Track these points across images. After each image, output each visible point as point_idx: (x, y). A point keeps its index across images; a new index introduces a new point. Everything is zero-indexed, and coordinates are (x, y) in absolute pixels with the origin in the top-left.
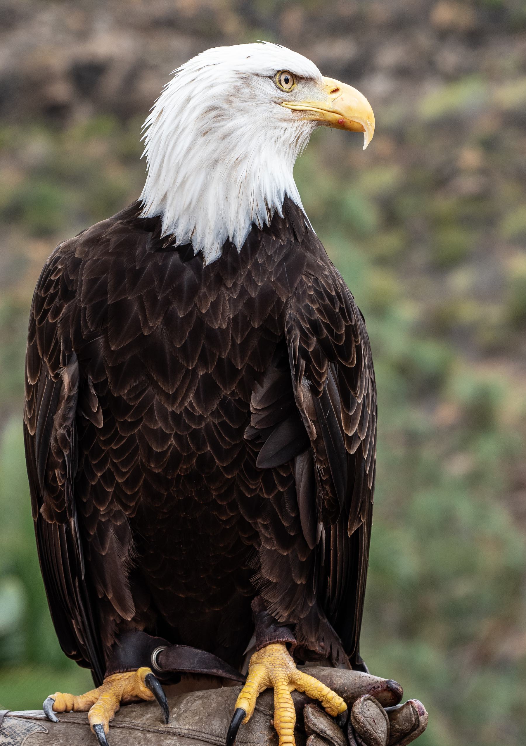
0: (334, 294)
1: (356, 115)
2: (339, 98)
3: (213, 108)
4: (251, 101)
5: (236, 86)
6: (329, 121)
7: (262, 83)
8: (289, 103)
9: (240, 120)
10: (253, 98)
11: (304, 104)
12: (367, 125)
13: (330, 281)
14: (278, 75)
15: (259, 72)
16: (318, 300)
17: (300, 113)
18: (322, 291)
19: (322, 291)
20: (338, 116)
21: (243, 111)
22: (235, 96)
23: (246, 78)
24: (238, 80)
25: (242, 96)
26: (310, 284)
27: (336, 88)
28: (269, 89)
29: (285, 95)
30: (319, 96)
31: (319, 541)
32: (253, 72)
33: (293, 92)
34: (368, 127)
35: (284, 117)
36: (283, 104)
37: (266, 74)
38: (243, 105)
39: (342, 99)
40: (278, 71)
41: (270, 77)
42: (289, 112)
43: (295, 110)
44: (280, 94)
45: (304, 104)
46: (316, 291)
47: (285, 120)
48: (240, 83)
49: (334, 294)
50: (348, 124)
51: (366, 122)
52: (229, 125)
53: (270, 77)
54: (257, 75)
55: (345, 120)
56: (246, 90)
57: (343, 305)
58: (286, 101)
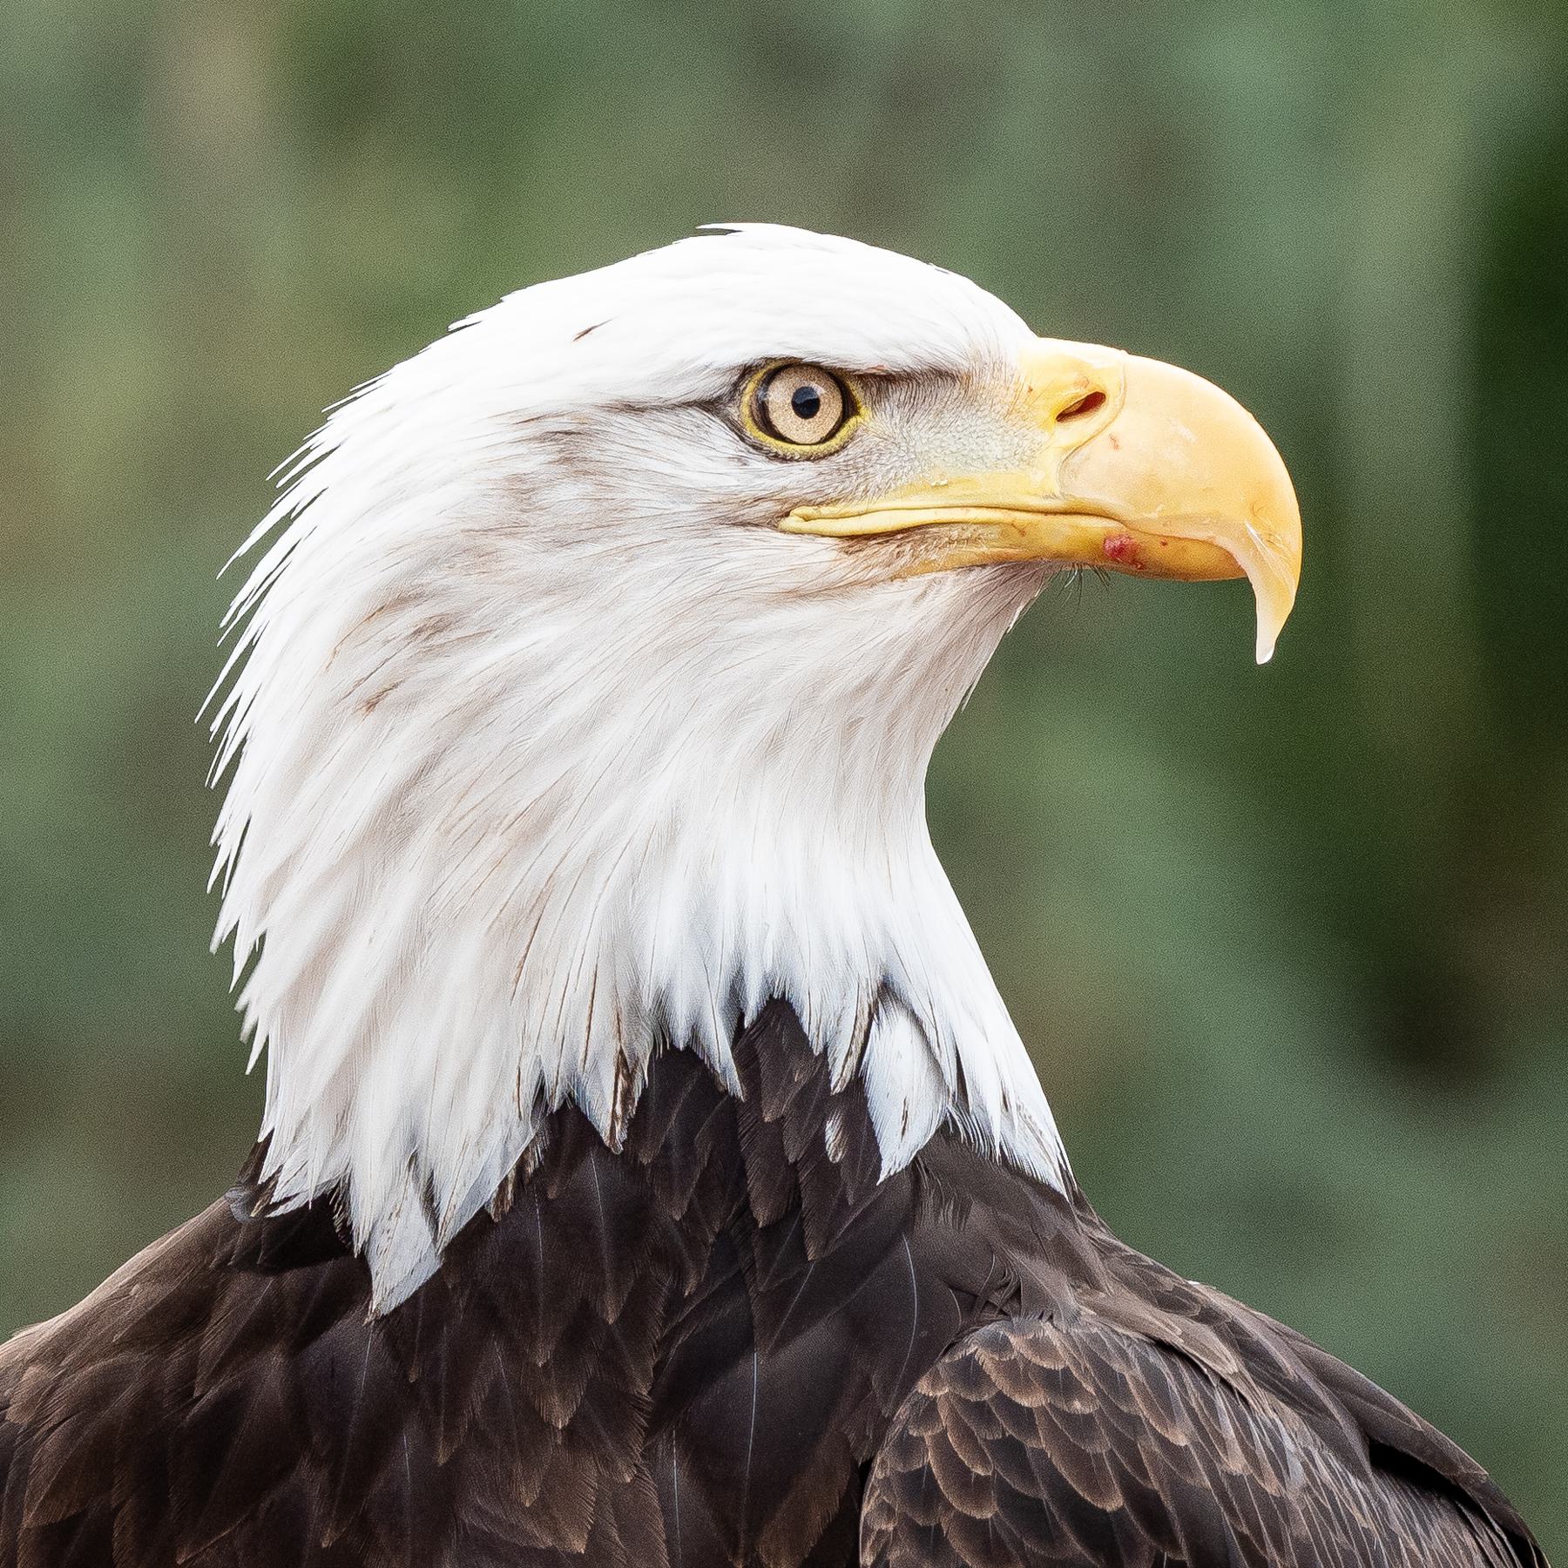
0: (1115, 1502)
1: (1188, 508)
2: (1102, 440)
3: (399, 601)
4: (596, 540)
5: (518, 478)
6: (1058, 555)
7: (657, 442)
8: (825, 510)
9: (539, 634)
10: (607, 521)
11: (915, 501)
12: (1250, 543)
13: (1101, 1446)
14: (750, 387)
15: (634, 394)
16: (1020, 1546)
17: (892, 547)
18: (1044, 1496)
19: (1044, 1496)
20: (1095, 527)
21: (562, 589)
22: (512, 530)
23: (568, 439)
24: (522, 449)
25: (546, 520)
26: (980, 1471)
27: (1084, 393)
28: (712, 461)
29: (797, 477)
30: (996, 449)
31: (243, 549)
32: (601, 401)
33: (852, 450)
34: (1258, 557)
35: (789, 583)
36: (791, 522)
37: (675, 393)
38: (560, 562)
39: (1113, 439)
40: (747, 371)
41: (710, 405)
42: (820, 557)
43: (858, 540)
44: (765, 477)
45: (915, 501)
46: (1009, 1499)
47: (799, 595)
48: (535, 462)
49: (1115, 1502)
50: (1157, 552)
51: (1245, 534)
52: (480, 663)
53: (710, 405)
54: (631, 408)
55: (1137, 539)
56: (568, 495)
57: (1174, 1546)
58: (809, 503)
